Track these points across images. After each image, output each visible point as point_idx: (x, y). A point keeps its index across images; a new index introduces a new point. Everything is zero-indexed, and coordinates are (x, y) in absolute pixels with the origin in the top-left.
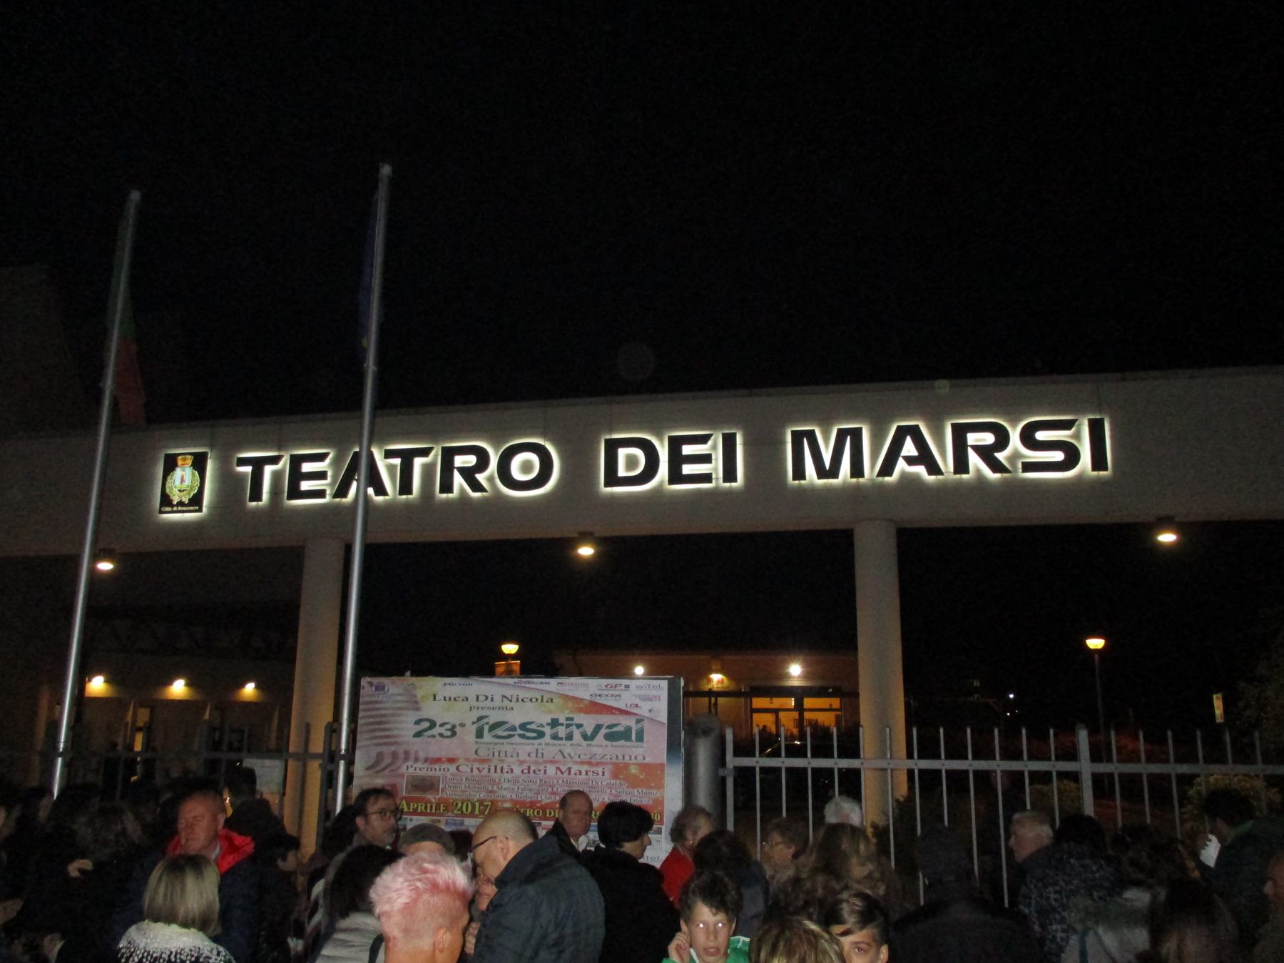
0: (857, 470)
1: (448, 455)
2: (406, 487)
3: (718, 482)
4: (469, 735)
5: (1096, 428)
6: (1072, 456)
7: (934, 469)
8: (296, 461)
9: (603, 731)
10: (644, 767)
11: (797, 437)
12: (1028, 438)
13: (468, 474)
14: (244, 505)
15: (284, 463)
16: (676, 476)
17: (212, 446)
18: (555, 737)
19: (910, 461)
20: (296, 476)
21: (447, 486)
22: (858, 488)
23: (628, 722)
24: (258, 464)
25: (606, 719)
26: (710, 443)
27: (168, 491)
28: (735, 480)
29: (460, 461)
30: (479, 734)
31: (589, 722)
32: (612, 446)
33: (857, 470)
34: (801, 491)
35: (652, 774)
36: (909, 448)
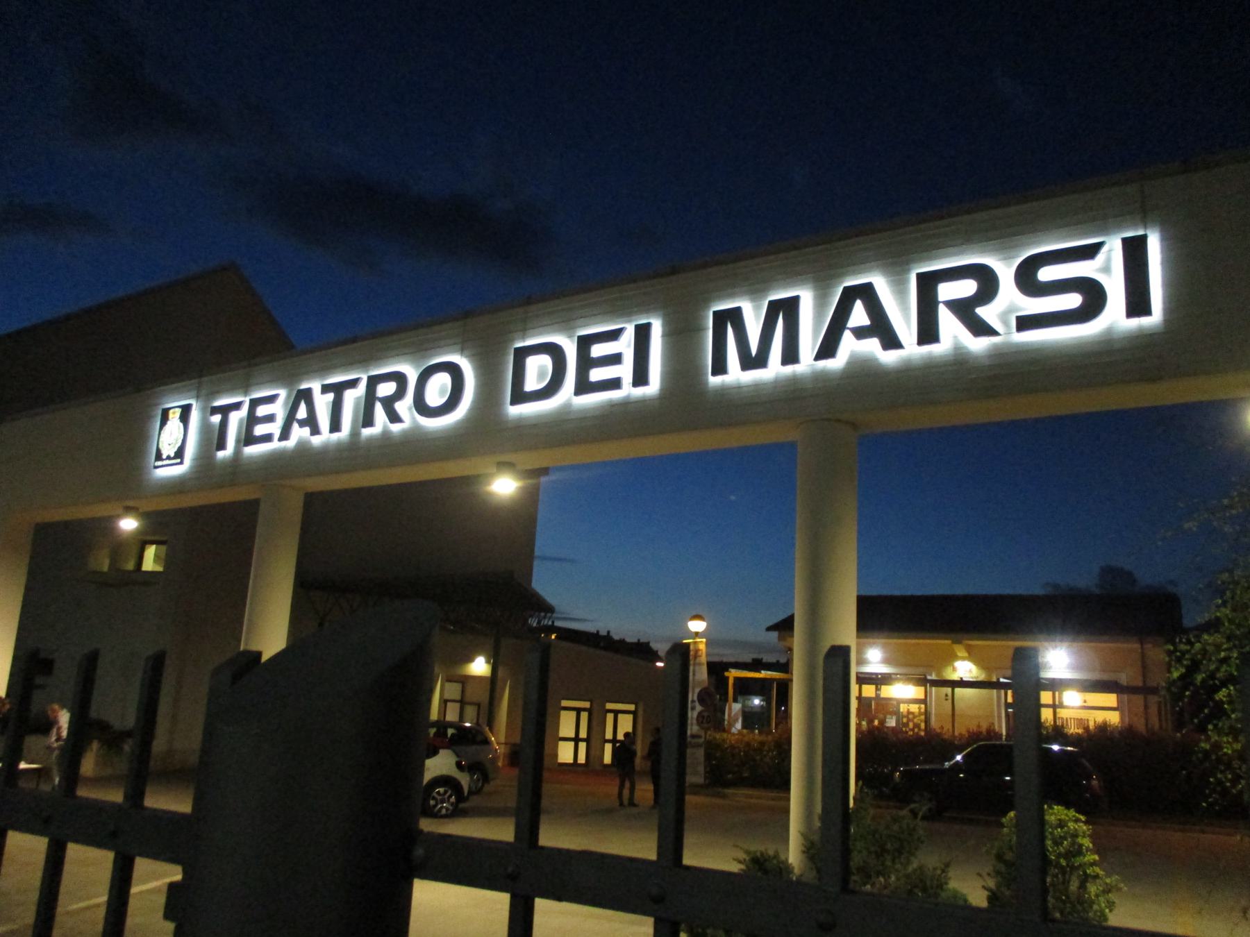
0: (791, 355)
1: (373, 382)
2: (335, 426)
3: (628, 391)
5: (1135, 253)
6: (1094, 296)
7: (891, 341)
8: (255, 403)
12: (1027, 280)
13: (389, 403)
14: (706, 383)
16: (584, 386)
17: (198, 397)
19: (860, 333)
20: (252, 420)
22: (794, 381)
26: (1101, 257)
27: (160, 446)
28: (1147, 311)
29: (948, 291)
32: (521, 354)
33: (791, 355)
34: (723, 391)
36: (859, 316)
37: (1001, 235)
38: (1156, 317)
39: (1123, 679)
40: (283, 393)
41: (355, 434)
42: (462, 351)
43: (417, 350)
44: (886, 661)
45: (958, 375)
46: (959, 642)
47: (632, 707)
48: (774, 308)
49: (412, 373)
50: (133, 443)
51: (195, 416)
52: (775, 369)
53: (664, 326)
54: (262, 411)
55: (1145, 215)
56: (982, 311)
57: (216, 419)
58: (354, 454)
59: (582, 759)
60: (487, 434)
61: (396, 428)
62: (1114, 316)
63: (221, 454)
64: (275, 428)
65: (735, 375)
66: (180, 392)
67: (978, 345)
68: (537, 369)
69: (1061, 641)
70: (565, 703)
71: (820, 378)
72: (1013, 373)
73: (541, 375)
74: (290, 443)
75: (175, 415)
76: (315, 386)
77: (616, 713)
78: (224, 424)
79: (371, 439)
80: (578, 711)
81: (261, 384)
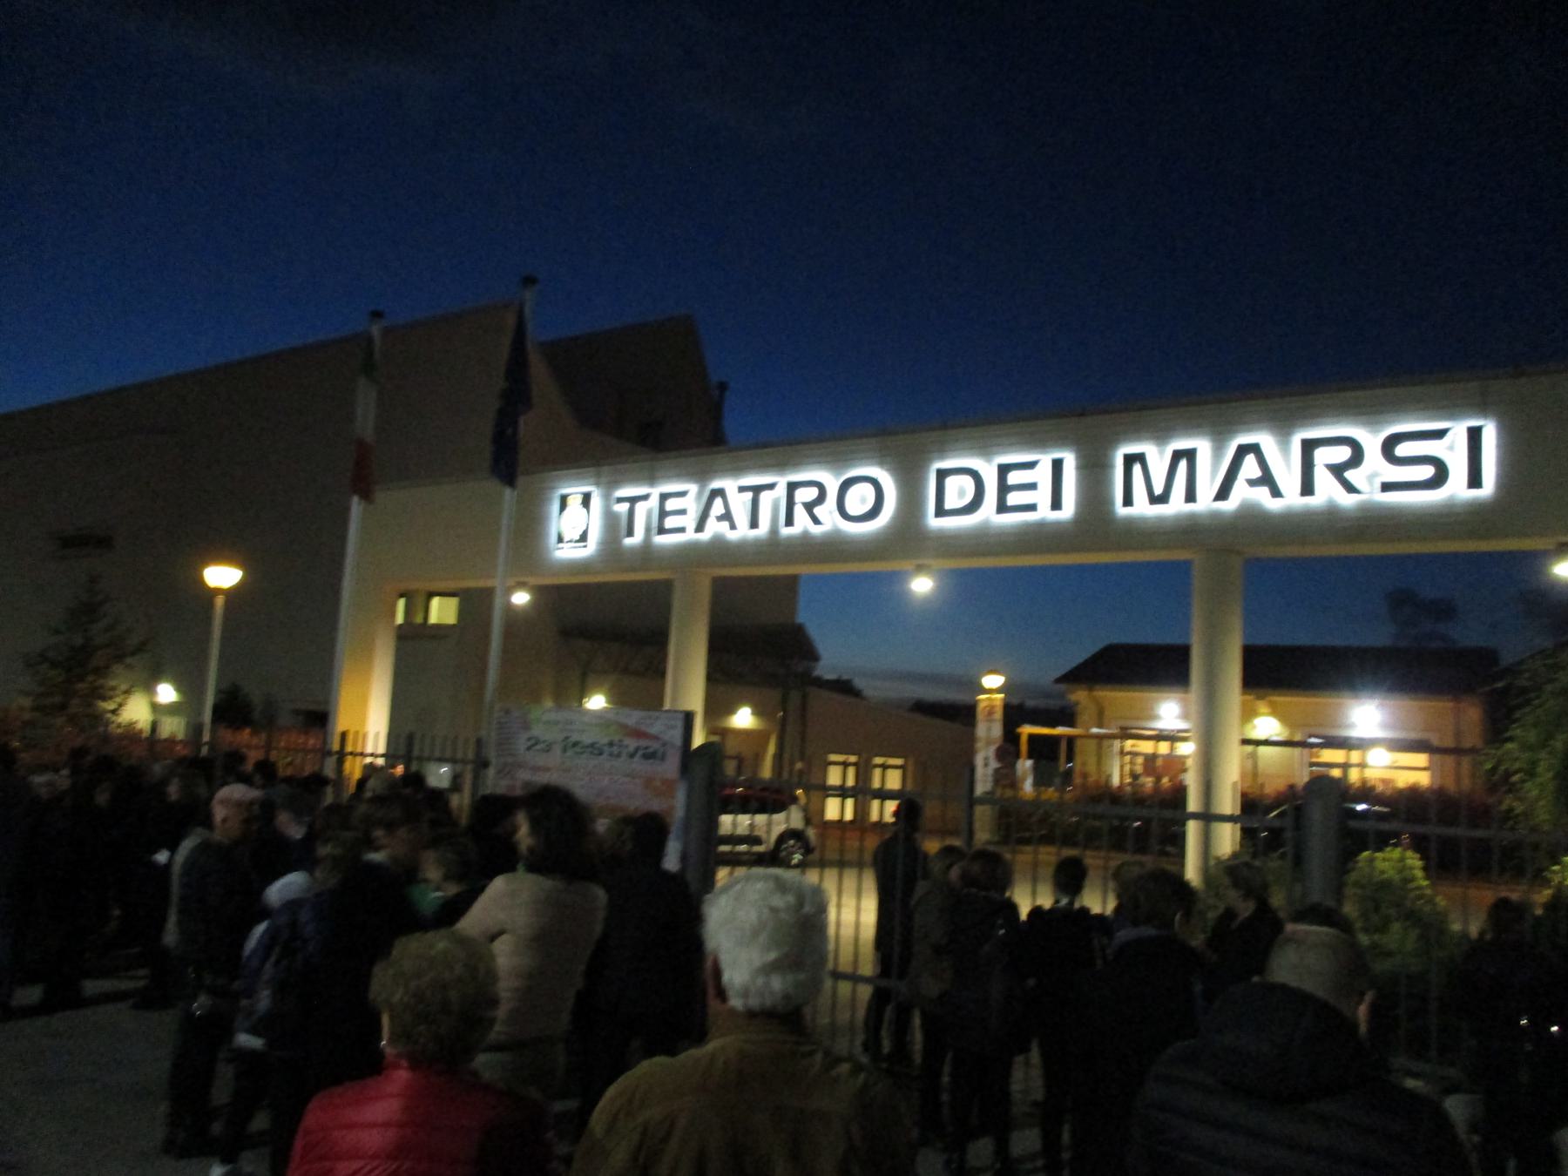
0: (1191, 496)
1: (792, 487)
2: (754, 524)
3: (1045, 513)
4: (557, 750)
8: (664, 497)
9: (640, 753)
10: (665, 782)
11: (1130, 460)
13: (809, 507)
15: (654, 502)
16: (1002, 507)
17: (597, 484)
18: (611, 755)
19: (1252, 483)
20: (663, 514)
21: (789, 521)
23: (655, 746)
24: (633, 500)
25: (643, 743)
30: (565, 750)
31: (632, 744)
32: (942, 475)
33: (1191, 496)
35: (668, 788)
36: (1250, 467)
37: (1370, 412)
38: (1488, 487)
39: (1436, 742)
40: (692, 488)
41: (774, 530)
42: (881, 464)
43: (837, 460)
44: (1185, 716)
45: (1331, 523)
46: (1259, 698)
47: (899, 762)
48: (1177, 456)
49: (832, 482)
50: (530, 526)
51: (596, 502)
52: (1176, 505)
53: (1077, 458)
54: (671, 505)
55: (1483, 409)
56: (1349, 475)
57: (623, 508)
58: (773, 548)
59: (849, 816)
60: (907, 539)
61: (816, 530)
62: (1456, 488)
63: (628, 541)
64: (689, 521)
65: (1141, 507)
66: (580, 479)
67: (1346, 500)
68: (958, 491)
69: (1371, 697)
70: (833, 757)
71: (1215, 516)
72: (1373, 523)
73: (962, 493)
74: (705, 536)
75: (575, 502)
76: (729, 484)
77: (885, 767)
78: (631, 513)
79: (790, 538)
80: (845, 765)
81: (669, 478)
